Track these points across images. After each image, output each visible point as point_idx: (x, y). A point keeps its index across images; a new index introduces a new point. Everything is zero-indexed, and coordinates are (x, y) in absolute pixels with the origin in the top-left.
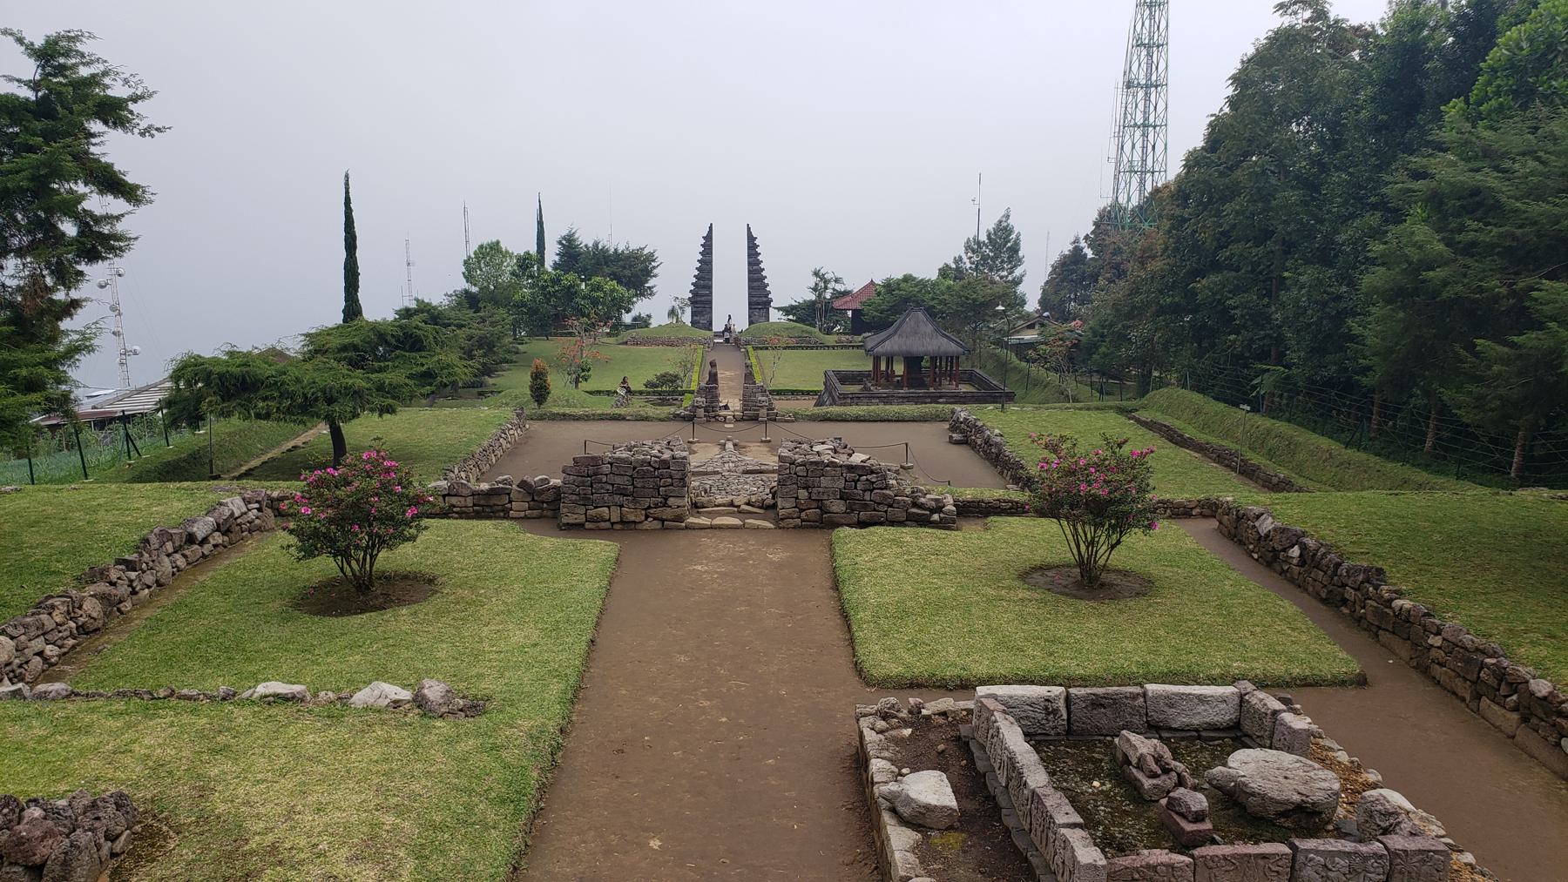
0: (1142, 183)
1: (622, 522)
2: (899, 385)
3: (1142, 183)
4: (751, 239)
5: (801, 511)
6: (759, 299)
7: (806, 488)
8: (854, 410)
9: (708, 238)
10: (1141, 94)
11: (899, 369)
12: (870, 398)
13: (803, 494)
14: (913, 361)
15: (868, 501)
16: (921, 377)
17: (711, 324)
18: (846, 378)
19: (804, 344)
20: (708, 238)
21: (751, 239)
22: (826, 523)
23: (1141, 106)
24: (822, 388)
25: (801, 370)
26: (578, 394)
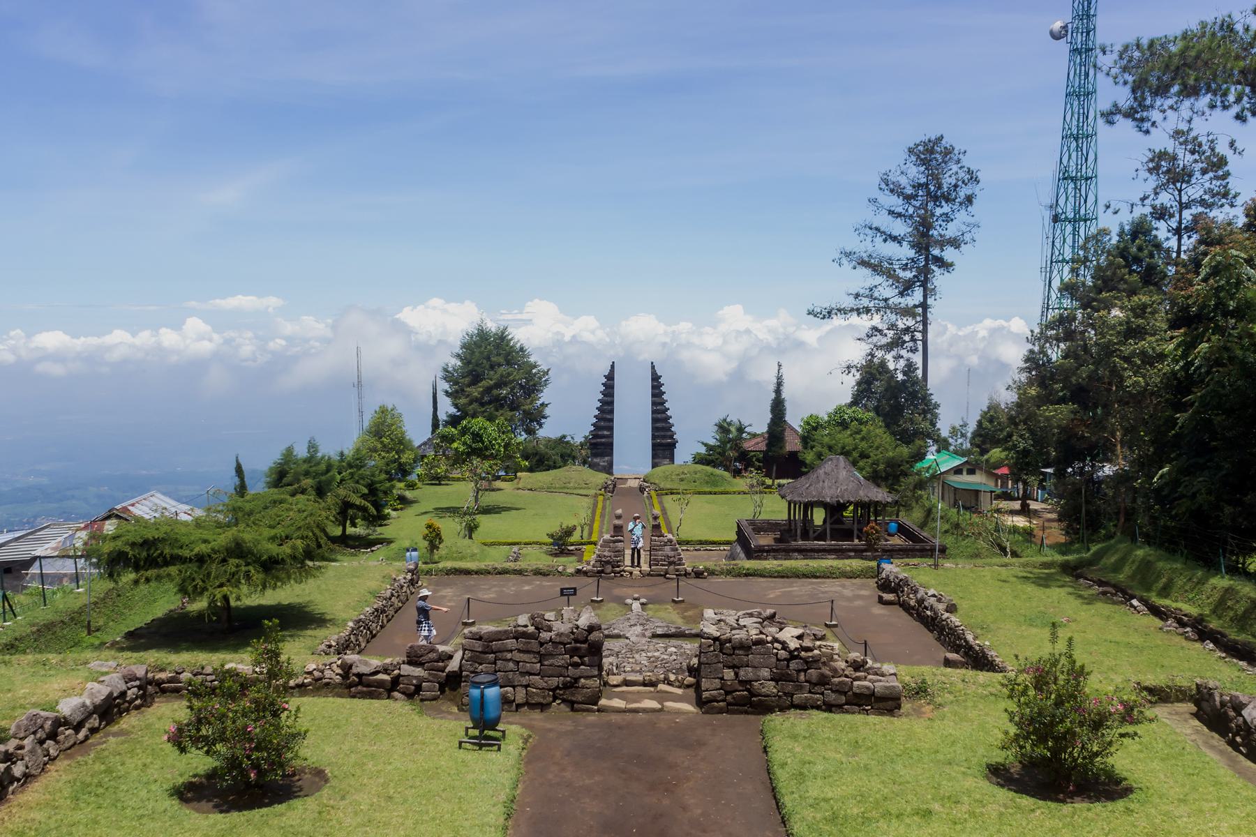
0: (1075, 232)
1: (527, 704)
2: (821, 537)
3: (1075, 232)
4: (656, 378)
5: (727, 693)
6: (663, 446)
7: (733, 667)
8: (770, 564)
9: (610, 377)
10: (1069, 228)
11: (819, 516)
12: (787, 553)
13: (729, 674)
14: (834, 509)
15: (809, 684)
16: (847, 528)
17: (611, 464)
18: (760, 527)
19: (712, 489)
20: (610, 377)
21: (656, 378)
22: (750, 703)
23: (1069, 240)
24: (733, 536)
25: (709, 517)
26: (472, 546)
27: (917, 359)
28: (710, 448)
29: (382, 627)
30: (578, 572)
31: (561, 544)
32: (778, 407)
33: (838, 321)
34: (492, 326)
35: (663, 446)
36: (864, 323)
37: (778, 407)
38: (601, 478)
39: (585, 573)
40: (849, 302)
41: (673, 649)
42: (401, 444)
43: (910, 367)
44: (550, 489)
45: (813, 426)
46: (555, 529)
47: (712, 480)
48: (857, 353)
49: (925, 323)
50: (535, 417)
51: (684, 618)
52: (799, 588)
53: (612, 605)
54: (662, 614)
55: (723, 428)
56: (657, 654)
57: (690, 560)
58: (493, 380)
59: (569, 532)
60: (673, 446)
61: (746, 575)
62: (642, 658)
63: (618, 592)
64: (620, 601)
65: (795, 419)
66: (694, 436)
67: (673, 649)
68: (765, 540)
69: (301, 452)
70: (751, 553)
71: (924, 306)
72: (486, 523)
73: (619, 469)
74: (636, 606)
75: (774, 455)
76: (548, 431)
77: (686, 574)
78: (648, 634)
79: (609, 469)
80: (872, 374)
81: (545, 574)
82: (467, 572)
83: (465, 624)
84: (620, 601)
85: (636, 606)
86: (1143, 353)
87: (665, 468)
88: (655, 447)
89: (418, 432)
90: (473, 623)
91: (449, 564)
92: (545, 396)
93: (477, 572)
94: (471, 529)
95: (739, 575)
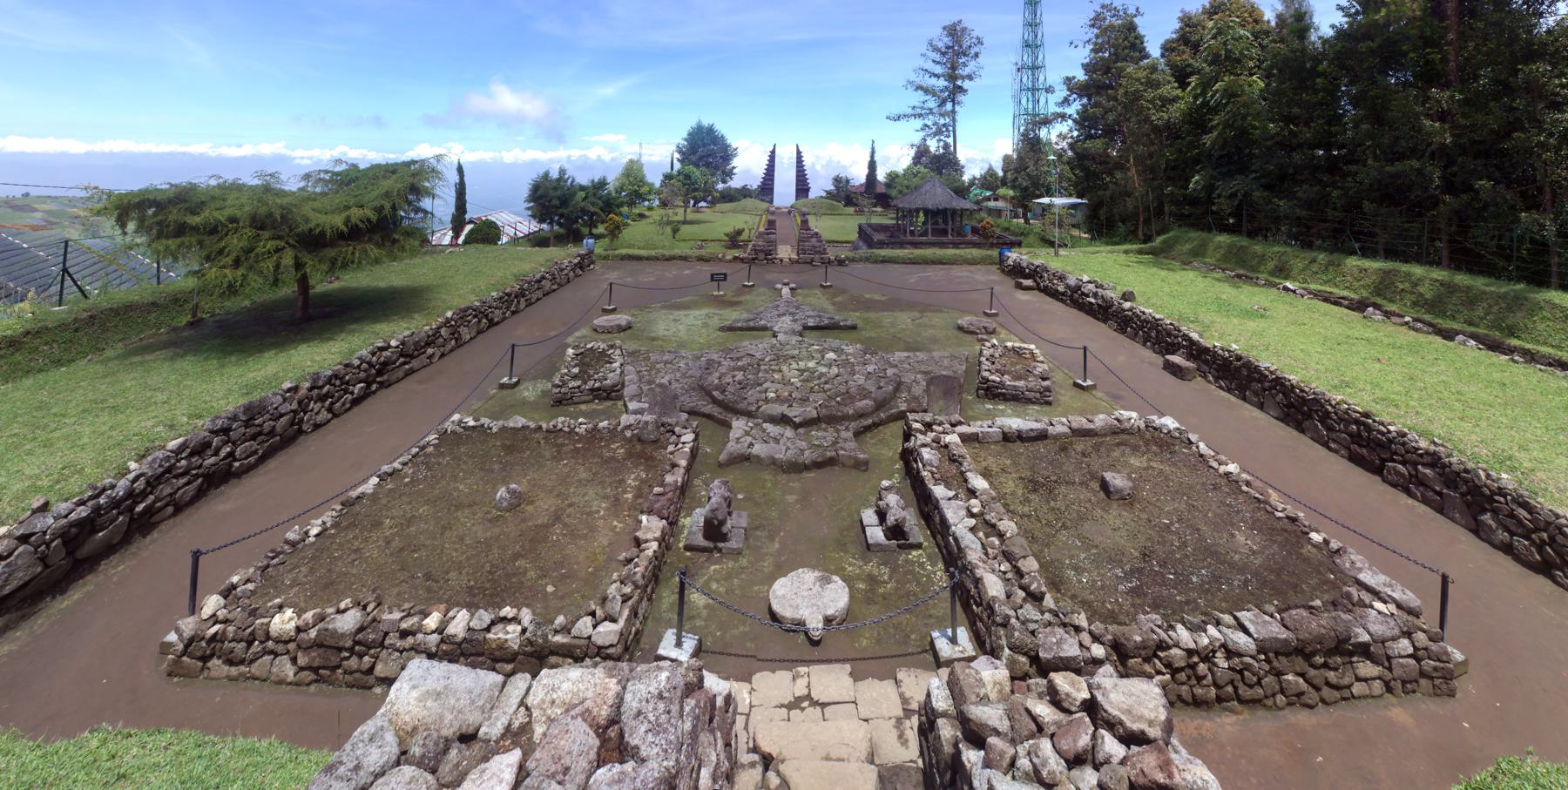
2: (925, 234)
6: (802, 187)
8: (884, 252)
9: (773, 152)
19: (832, 212)
24: (854, 236)
25: (839, 228)
27: (950, 140)
28: (828, 193)
29: (514, 313)
30: (736, 258)
31: (734, 240)
32: (872, 166)
33: (902, 122)
34: (706, 123)
35: (802, 187)
36: (918, 123)
37: (872, 166)
38: (765, 205)
39: (742, 260)
40: (910, 111)
41: (831, 355)
42: (641, 181)
43: (946, 146)
44: (734, 211)
45: (893, 177)
46: (730, 229)
47: (832, 208)
48: (917, 138)
49: (954, 120)
50: (729, 174)
51: (834, 304)
52: (915, 276)
53: (762, 289)
54: (812, 300)
55: (837, 180)
56: (811, 364)
57: (831, 254)
58: (706, 152)
59: (739, 232)
60: (808, 190)
61: (883, 262)
62: (791, 371)
63: (770, 276)
64: (771, 286)
65: (881, 176)
66: (820, 186)
67: (831, 355)
68: (877, 237)
69: (555, 175)
70: (870, 244)
71: (953, 112)
72: (685, 229)
73: (777, 202)
74: (786, 291)
75: (876, 193)
76: (735, 183)
77: (830, 262)
78: (798, 327)
79: (771, 201)
80: (921, 153)
81: (707, 261)
82: (639, 258)
83: (606, 312)
84: (771, 286)
85: (786, 291)
86: (1161, 98)
87: (803, 201)
88: (798, 190)
89: (655, 179)
90: (613, 311)
91: (624, 251)
92: (735, 162)
93: (648, 259)
94: (675, 231)
95: (876, 262)
